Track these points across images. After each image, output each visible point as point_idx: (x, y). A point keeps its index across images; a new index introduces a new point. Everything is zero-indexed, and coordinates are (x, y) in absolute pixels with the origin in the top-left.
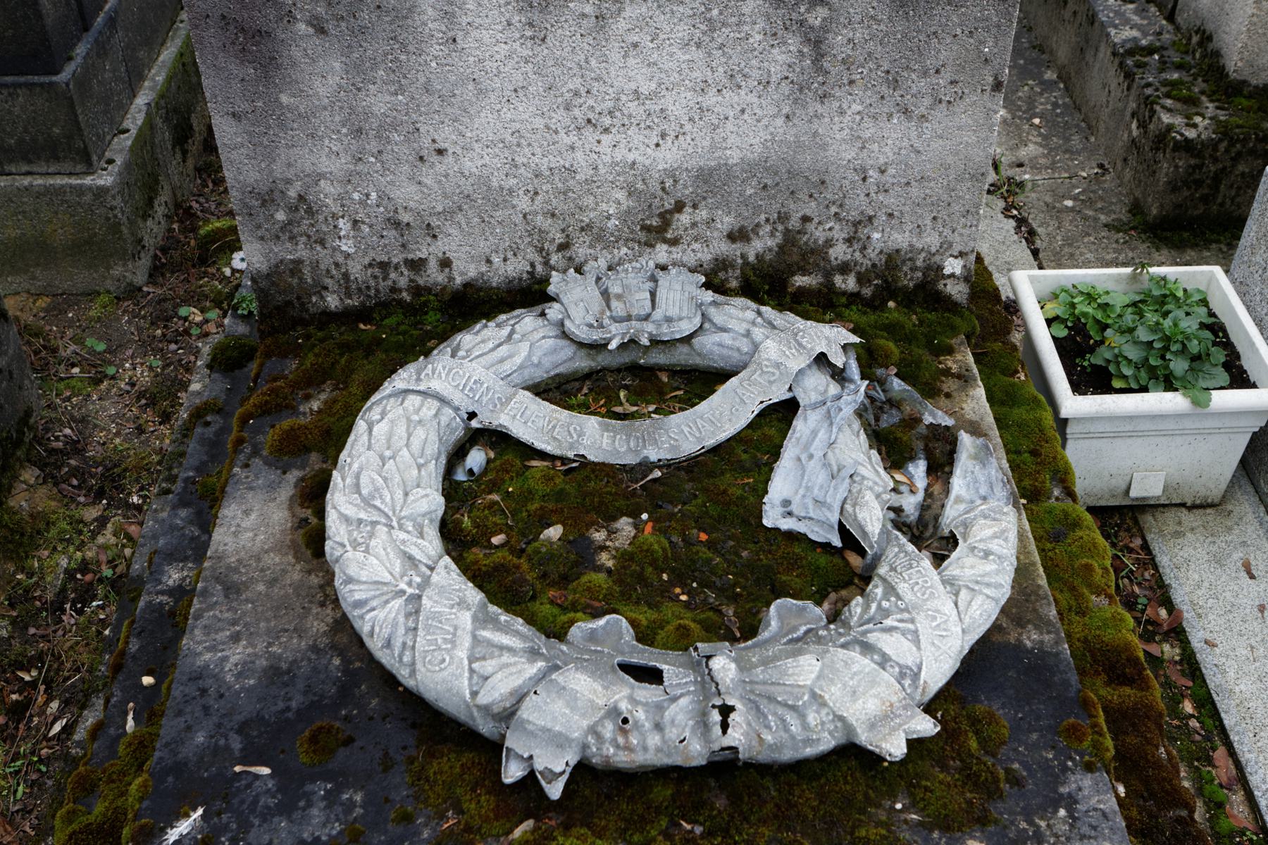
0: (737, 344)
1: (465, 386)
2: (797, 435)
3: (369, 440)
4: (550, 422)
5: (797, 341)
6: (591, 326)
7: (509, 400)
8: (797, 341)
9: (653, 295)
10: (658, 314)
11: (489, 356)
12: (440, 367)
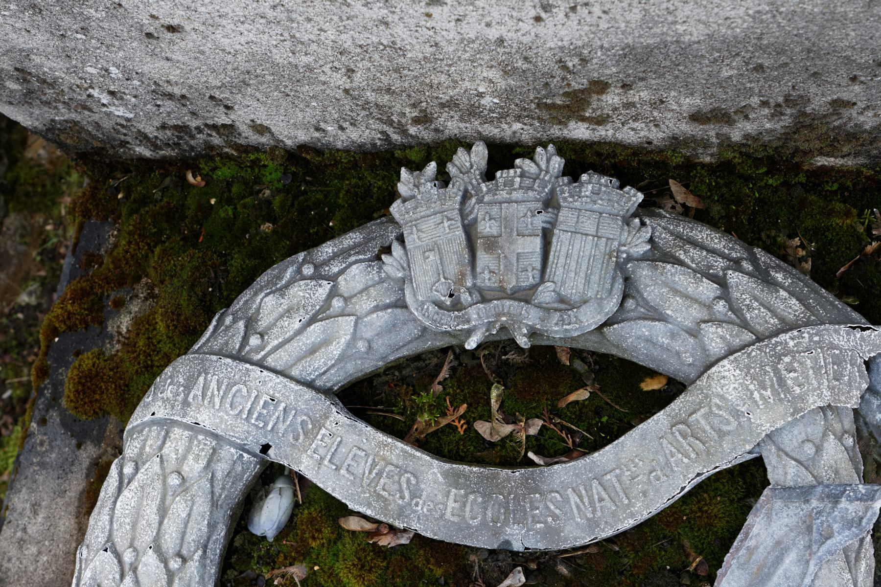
0: (677, 346)
1: (250, 412)
2: (751, 543)
3: (111, 521)
4: (374, 464)
5: (776, 371)
6: (439, 305)
7: (318, 425)
8: (776, 371)
9: (547, 237)
10: (546, 294)
11: (294, 343)
12: (213, 385)
